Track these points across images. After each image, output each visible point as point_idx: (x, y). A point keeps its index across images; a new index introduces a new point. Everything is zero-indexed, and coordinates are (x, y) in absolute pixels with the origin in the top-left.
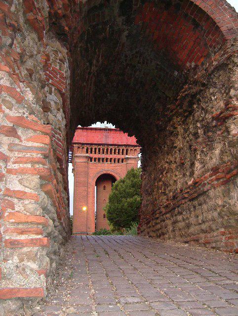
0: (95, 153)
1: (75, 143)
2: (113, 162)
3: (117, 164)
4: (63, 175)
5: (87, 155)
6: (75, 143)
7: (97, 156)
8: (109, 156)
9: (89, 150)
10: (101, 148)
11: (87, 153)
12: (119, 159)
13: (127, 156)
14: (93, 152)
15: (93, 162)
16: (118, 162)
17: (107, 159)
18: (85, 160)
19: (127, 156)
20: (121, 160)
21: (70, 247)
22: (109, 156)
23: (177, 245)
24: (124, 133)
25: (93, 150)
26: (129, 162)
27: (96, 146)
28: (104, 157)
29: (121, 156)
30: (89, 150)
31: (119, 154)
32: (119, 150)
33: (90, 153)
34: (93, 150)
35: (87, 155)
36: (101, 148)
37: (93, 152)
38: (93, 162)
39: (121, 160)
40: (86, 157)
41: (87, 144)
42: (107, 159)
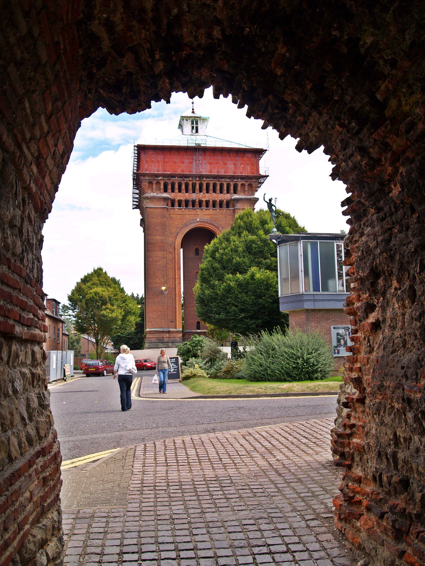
5: (165, 195)
8: (204, 196)
10: (190, 183)
11: (165, 191)
13: (236, 196)
14: (177, 190)
15: (176, 207)
16: (193, 206)
17: (200, 202)
18: (161, 205)
19: (236, 196)
21: (335, 467)
22: (204, 196)
23: (91, 511)
24: (334, 175)
26: (238, 206)
27: (215, 181)
29: (226, 197)
31: (214, 191)
33: (170, 191)
35: (165, 195)
36: (190, 183)
37: (177, 190)
38: (176, 207)
40: (165, 199)
41: (164, 176)
42: (214, 203)
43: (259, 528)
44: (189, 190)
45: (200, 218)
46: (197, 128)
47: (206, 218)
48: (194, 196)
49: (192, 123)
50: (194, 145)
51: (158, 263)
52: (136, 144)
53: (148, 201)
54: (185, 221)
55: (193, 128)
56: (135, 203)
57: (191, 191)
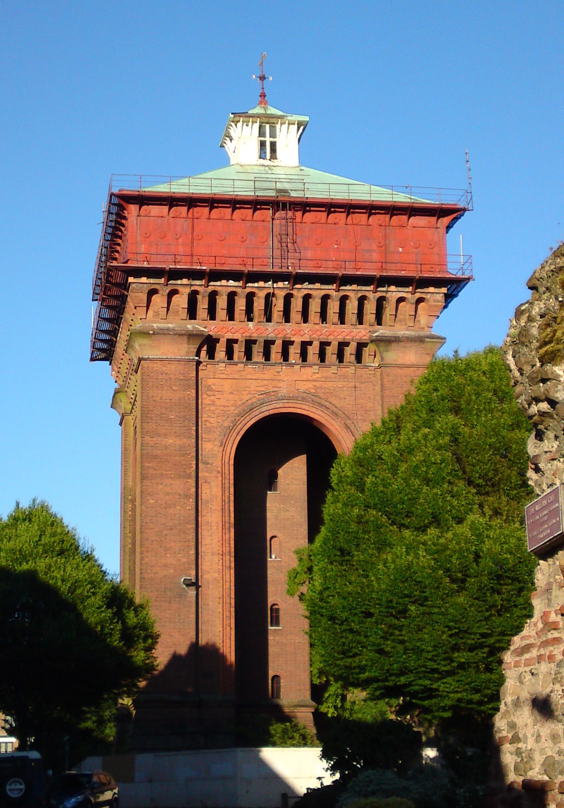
0: (306, 320)
1: (138, 272)
2: (258, 356)
3: (333, 368)
4: (273, 118)
5: (190, 326)
6: (138, 272)
7: (240, 329)
8: (298, 331)
9: (203, 305)
12: (250, 343)
13: (382, 331)
14: (221, 313)
16: (267, 355)
20: (350, 351)
22: (298, 331)
25: (222, 302)
26: (393, 355)
28: (271, 336)
30: (203, 305)
32: (250, 297)
34: (222, 302)
35: (190, 326)
39: (350, 351)
40: (191, 336)
43: (473, 561)
44: (237, 316)
45: (289, 387)
46: (273, 145)
47: (303, 387)
48: (274, 330)
49: (261, 133)
50: (273, 194)
51: (171, 511)
52: (115, 191)
53: (145, 341)
54: (246, 398)
55: (263, 144)
56: (99, 345)
57: (243, 317)
